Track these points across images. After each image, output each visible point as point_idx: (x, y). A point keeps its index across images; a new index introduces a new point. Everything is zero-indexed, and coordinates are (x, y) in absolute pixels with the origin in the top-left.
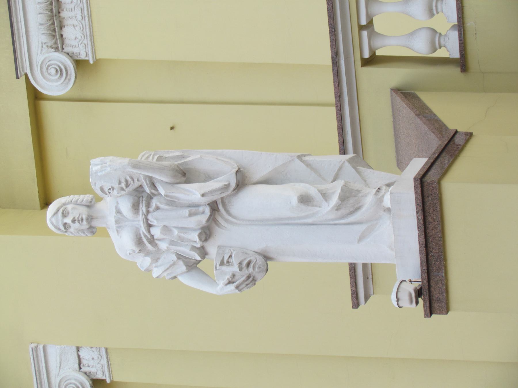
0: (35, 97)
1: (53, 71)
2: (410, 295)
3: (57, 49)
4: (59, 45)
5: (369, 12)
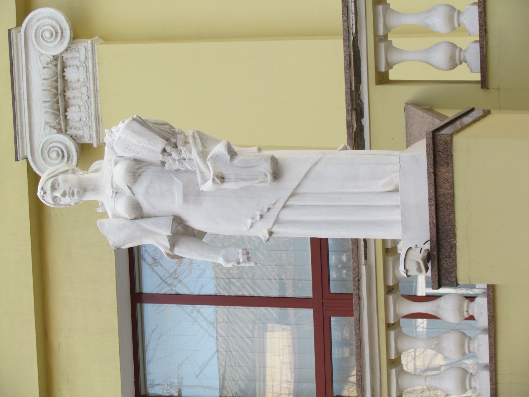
1: (54, 155)
2: (418, 263)
3: (60, 131)
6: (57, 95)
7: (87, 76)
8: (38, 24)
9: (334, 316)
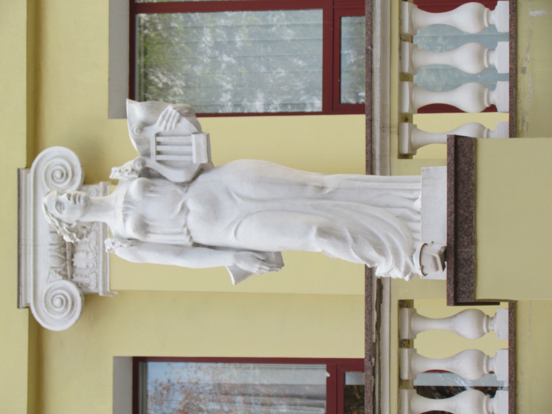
0: (37, 334)
1: (57, 302)
2: (435, 259)
3: (65, 277)
4: (69, 273)
5: (412, 408)
6: (66, 260)
7: (96, 261)
8: (49, 163)
9: (346, 15)
